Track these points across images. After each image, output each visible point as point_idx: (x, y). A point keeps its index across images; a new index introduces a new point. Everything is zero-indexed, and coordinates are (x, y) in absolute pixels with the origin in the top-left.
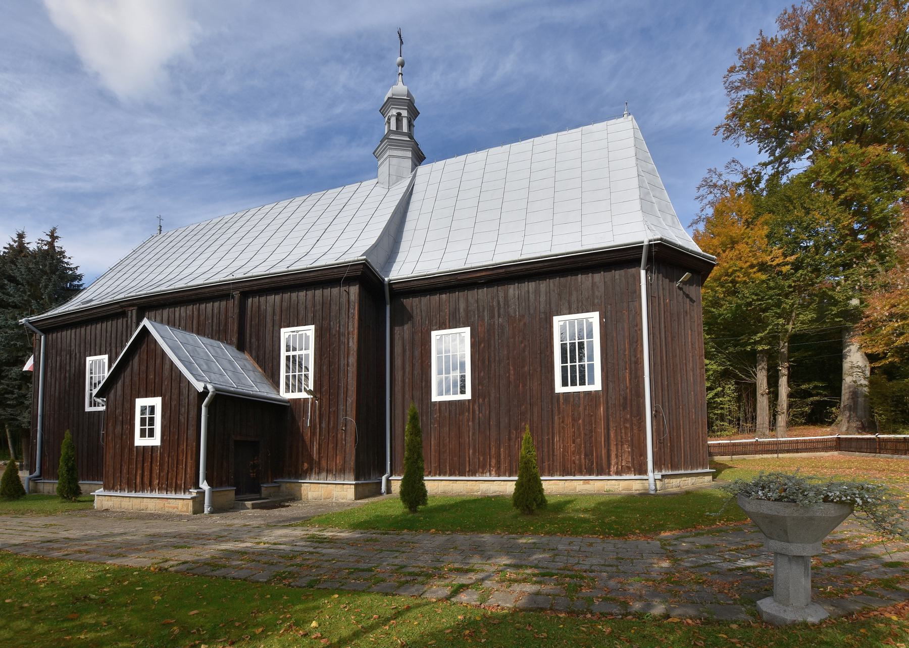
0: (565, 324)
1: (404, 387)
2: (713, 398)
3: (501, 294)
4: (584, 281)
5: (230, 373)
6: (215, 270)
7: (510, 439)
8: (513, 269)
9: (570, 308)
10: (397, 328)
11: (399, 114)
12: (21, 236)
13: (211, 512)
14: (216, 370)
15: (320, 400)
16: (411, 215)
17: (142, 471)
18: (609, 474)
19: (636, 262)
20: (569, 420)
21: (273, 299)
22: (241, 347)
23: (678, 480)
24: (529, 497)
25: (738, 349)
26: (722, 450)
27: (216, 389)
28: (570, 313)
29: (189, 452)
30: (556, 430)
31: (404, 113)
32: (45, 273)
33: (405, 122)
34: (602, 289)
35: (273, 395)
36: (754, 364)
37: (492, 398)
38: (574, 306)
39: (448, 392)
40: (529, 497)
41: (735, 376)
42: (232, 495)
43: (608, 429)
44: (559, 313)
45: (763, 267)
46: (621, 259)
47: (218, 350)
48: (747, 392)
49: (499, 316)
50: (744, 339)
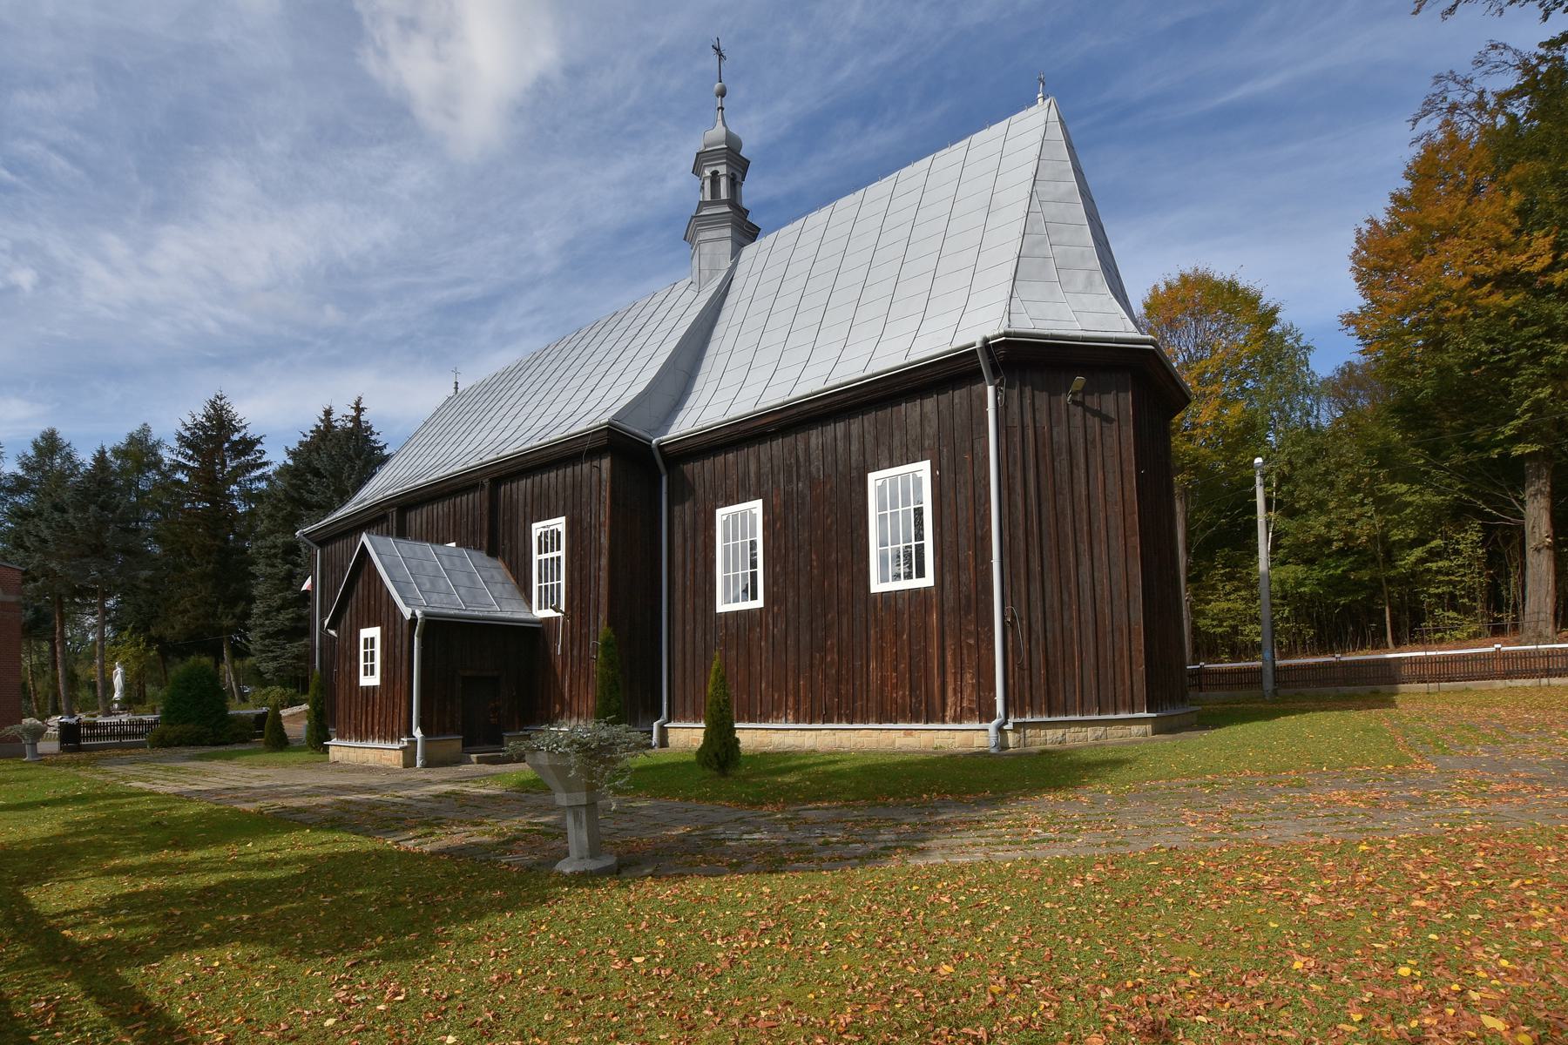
0: (884, 484)
1: (684, 592)
2: (1422, 561)
3: (801, 446)
4: (911, 411)
5: (462, 591)
6: (603, 406)
7: (811, 666)
8: (806, 407)
9: (891, 458)
10: (677, 509)
11: (715, 173)
12: (328, 413)
13: (425, 766)
14: (443, 587)
15: (572, 618)
16: (718, 331)
17: (374, 716)
18: (944, 721)
19: (974, 376)
20: (889, 636)
21: (524, 484)
22: (493, 552)
23: (1060, 732)
24: (721, 751)
25: (1473, 457)
26: (1417, 670)
27: (425, 614)
28: (891, 466)
29: (1109, 658)
30: (872, 653)
31: (722, 170)
32: (350, 459)
33: (723, 182)
34: (935, 423)
35: (529, 617)
36: (1519, 483)
37: (790, 605)
38: (897, 454)
39: (736, 600)
40: (721, 751)
41: (1479, 514)
42: (458, 745)
43: (942, 649)
44: (877, 467)
45: (1507, 280)
46: (948, 374)
47: (457, 561)
48: (1504, 547)
49: (798, 480)
50: (1480, 435)
